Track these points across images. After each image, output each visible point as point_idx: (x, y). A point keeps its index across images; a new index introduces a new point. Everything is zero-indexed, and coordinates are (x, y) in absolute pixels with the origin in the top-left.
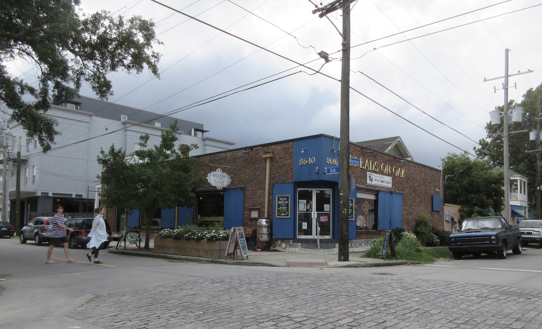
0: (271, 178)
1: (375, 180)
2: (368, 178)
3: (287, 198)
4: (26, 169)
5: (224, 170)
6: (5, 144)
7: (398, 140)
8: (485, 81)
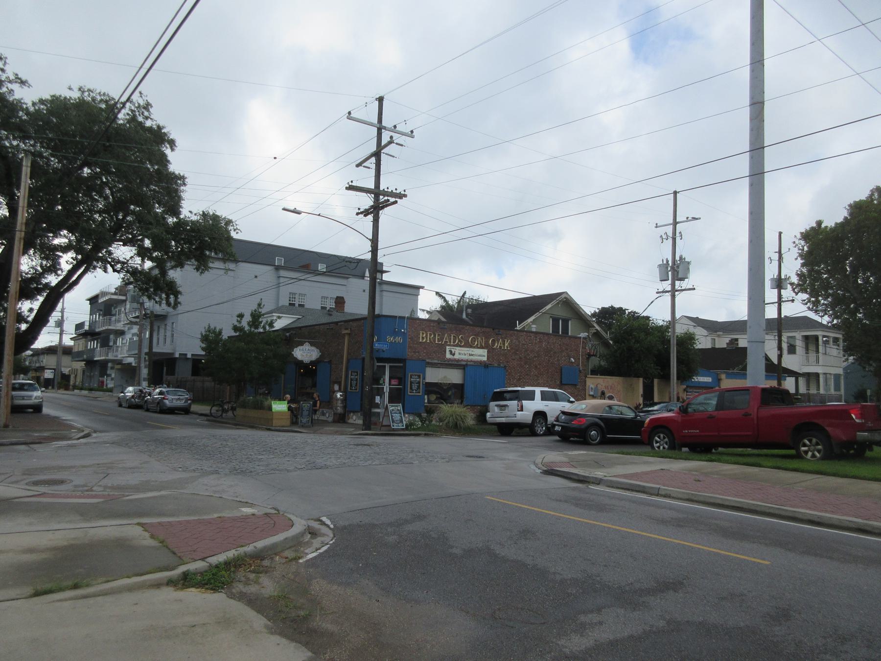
0: (348, 354)
2: (447, 351)
5: (312, 344)
7: (563, 296)
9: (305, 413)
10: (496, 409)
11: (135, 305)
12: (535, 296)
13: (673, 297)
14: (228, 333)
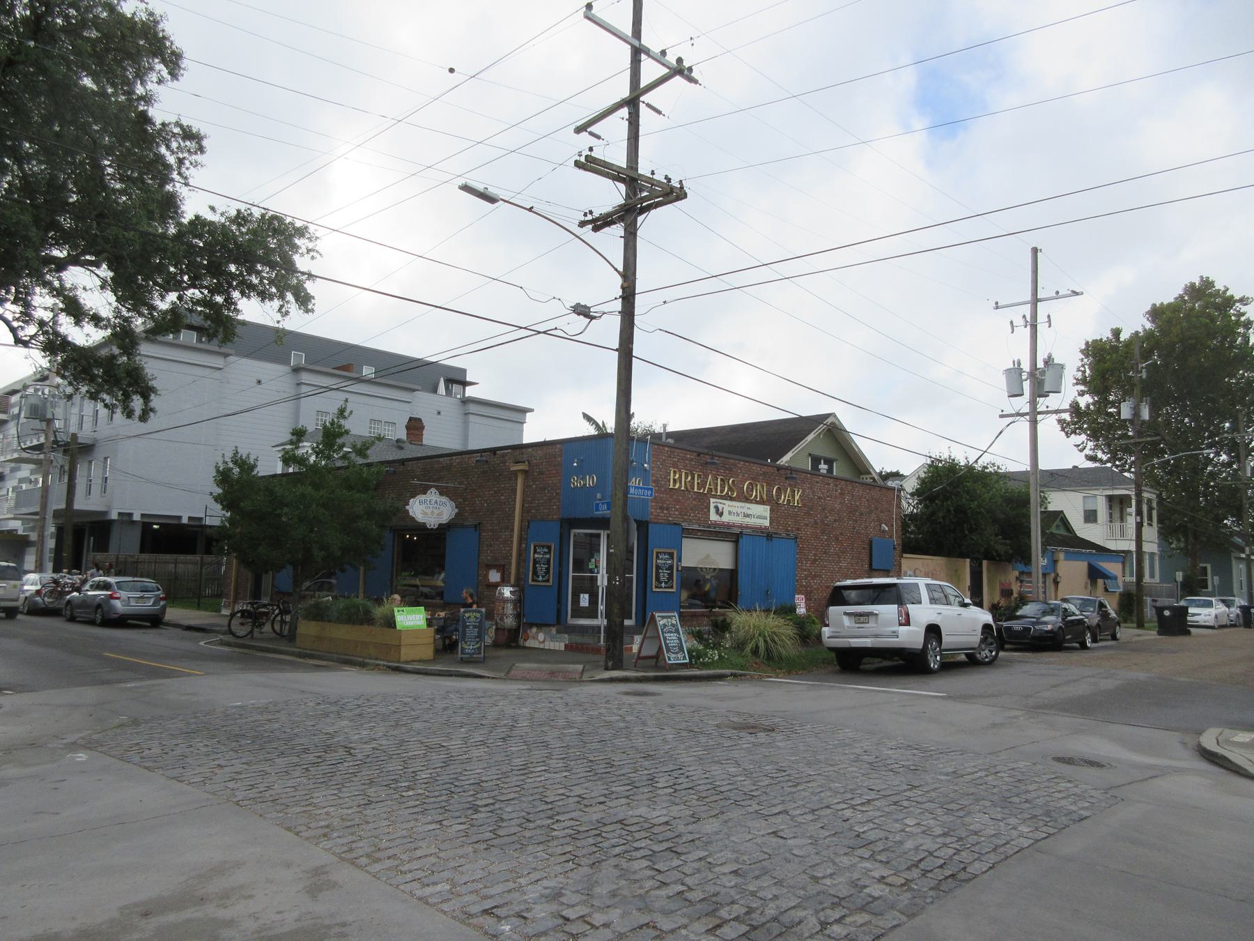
0: (525, 510)
1: (730, 513)
2: (712, 510)
4: (90, 462)
6: (49, 416)
7: (830, 420)
9: (472, 632)
10: (847, 621)
11: (37, 424)
13: (1034, 423)
14: (270, 465)
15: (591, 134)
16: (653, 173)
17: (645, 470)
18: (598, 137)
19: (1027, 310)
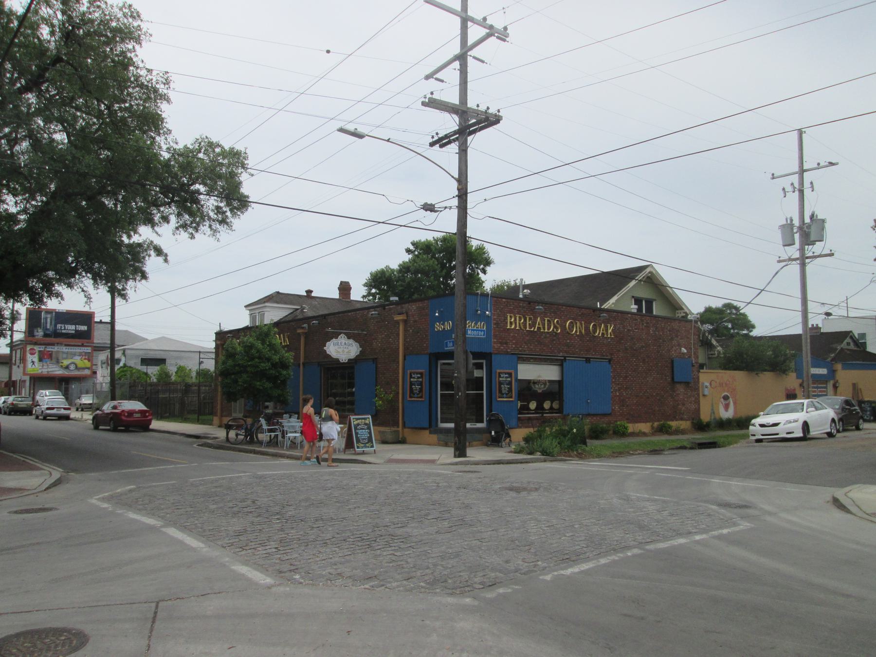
3: (421, 374)
7: (648, 270)
8: (773, 178)
12: (604, 274)
13: (803, 265)
15: (437, 79)
16: (478, 106)
17: (488, 316)
18: (442, 81)
19: (795, 179)
